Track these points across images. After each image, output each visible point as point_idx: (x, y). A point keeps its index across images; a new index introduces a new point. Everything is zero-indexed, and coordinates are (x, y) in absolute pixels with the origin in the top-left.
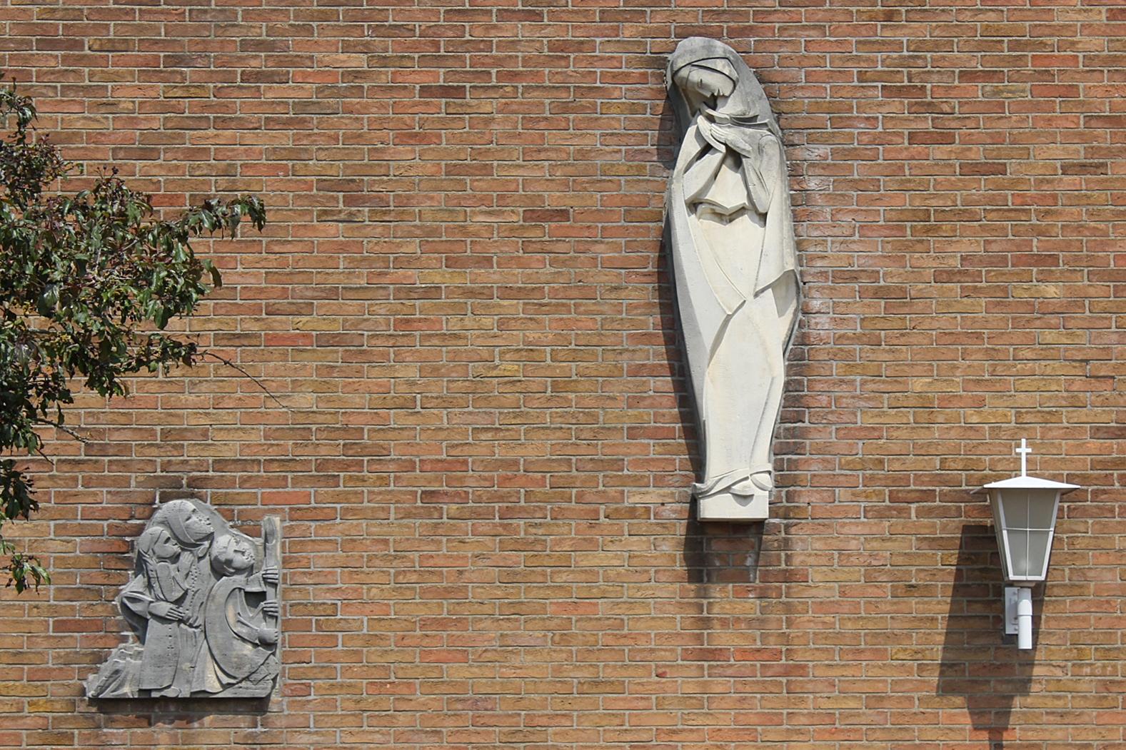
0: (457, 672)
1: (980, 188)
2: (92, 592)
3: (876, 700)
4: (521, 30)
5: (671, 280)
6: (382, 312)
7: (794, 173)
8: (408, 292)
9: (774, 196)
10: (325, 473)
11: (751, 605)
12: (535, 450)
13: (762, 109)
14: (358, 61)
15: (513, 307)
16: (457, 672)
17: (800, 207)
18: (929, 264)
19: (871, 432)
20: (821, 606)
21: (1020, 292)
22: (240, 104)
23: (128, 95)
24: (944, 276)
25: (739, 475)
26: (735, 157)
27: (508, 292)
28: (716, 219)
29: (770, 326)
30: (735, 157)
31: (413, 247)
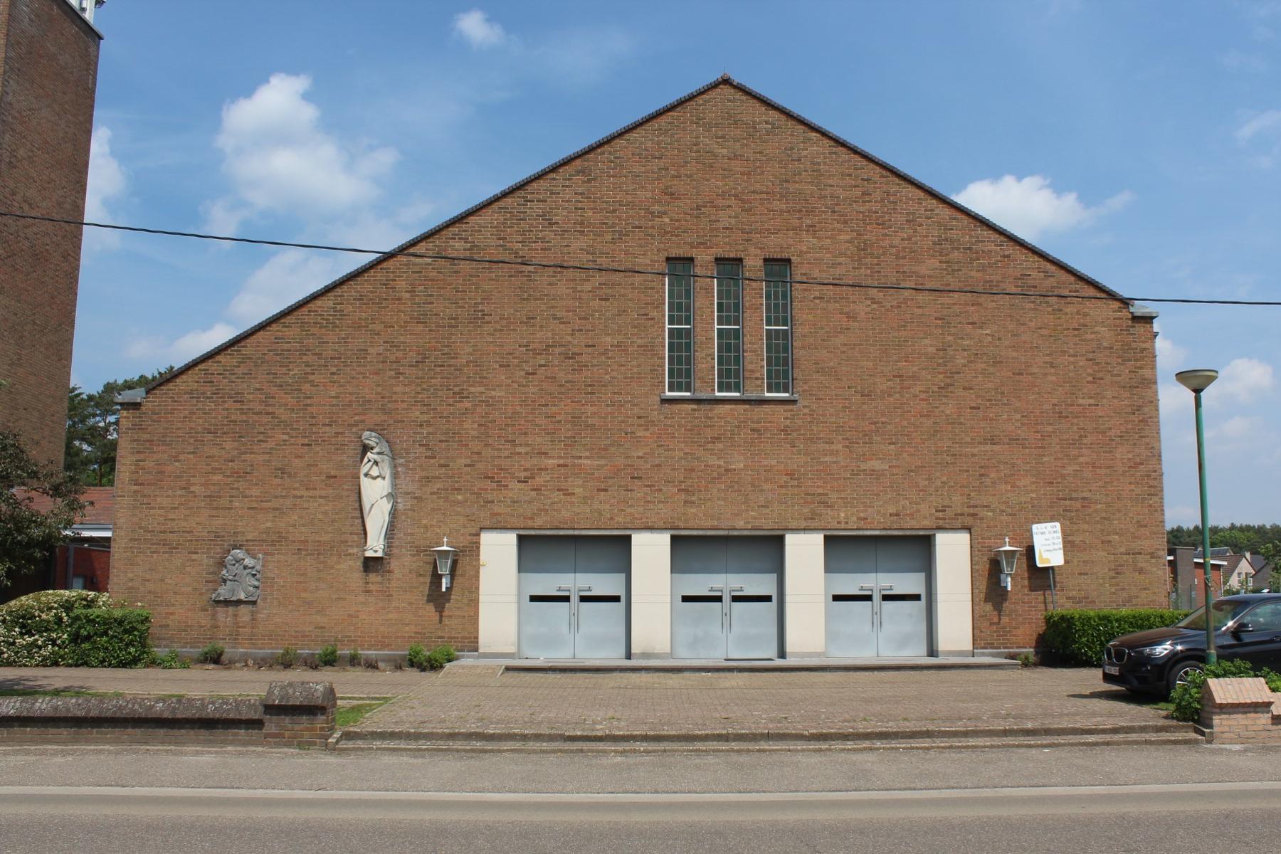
0: (304, 595)
1: (443, 470)
2: (214, 573)
3: (410, 604)
4: (327, 429)
5: (977, 632)
7: (395, 467)
8: (295, 497)
9: (387, 472)
10: (273, 544)
11: (379, 579)
12: (326, 538)
13: (386, 449)
14: (286, 437)
16: (304, 595)
17: (395, 475)
18: (429, 491)
19: (412, 534)
20: (398, 579)
21: (451, 498)
24: (432, 494)
25: (375, 545)
26: (376, 463)
27: (321, 497)
28: (983, 584)
29: (386, 506)
30: (376, 463)
31: (297, 485)
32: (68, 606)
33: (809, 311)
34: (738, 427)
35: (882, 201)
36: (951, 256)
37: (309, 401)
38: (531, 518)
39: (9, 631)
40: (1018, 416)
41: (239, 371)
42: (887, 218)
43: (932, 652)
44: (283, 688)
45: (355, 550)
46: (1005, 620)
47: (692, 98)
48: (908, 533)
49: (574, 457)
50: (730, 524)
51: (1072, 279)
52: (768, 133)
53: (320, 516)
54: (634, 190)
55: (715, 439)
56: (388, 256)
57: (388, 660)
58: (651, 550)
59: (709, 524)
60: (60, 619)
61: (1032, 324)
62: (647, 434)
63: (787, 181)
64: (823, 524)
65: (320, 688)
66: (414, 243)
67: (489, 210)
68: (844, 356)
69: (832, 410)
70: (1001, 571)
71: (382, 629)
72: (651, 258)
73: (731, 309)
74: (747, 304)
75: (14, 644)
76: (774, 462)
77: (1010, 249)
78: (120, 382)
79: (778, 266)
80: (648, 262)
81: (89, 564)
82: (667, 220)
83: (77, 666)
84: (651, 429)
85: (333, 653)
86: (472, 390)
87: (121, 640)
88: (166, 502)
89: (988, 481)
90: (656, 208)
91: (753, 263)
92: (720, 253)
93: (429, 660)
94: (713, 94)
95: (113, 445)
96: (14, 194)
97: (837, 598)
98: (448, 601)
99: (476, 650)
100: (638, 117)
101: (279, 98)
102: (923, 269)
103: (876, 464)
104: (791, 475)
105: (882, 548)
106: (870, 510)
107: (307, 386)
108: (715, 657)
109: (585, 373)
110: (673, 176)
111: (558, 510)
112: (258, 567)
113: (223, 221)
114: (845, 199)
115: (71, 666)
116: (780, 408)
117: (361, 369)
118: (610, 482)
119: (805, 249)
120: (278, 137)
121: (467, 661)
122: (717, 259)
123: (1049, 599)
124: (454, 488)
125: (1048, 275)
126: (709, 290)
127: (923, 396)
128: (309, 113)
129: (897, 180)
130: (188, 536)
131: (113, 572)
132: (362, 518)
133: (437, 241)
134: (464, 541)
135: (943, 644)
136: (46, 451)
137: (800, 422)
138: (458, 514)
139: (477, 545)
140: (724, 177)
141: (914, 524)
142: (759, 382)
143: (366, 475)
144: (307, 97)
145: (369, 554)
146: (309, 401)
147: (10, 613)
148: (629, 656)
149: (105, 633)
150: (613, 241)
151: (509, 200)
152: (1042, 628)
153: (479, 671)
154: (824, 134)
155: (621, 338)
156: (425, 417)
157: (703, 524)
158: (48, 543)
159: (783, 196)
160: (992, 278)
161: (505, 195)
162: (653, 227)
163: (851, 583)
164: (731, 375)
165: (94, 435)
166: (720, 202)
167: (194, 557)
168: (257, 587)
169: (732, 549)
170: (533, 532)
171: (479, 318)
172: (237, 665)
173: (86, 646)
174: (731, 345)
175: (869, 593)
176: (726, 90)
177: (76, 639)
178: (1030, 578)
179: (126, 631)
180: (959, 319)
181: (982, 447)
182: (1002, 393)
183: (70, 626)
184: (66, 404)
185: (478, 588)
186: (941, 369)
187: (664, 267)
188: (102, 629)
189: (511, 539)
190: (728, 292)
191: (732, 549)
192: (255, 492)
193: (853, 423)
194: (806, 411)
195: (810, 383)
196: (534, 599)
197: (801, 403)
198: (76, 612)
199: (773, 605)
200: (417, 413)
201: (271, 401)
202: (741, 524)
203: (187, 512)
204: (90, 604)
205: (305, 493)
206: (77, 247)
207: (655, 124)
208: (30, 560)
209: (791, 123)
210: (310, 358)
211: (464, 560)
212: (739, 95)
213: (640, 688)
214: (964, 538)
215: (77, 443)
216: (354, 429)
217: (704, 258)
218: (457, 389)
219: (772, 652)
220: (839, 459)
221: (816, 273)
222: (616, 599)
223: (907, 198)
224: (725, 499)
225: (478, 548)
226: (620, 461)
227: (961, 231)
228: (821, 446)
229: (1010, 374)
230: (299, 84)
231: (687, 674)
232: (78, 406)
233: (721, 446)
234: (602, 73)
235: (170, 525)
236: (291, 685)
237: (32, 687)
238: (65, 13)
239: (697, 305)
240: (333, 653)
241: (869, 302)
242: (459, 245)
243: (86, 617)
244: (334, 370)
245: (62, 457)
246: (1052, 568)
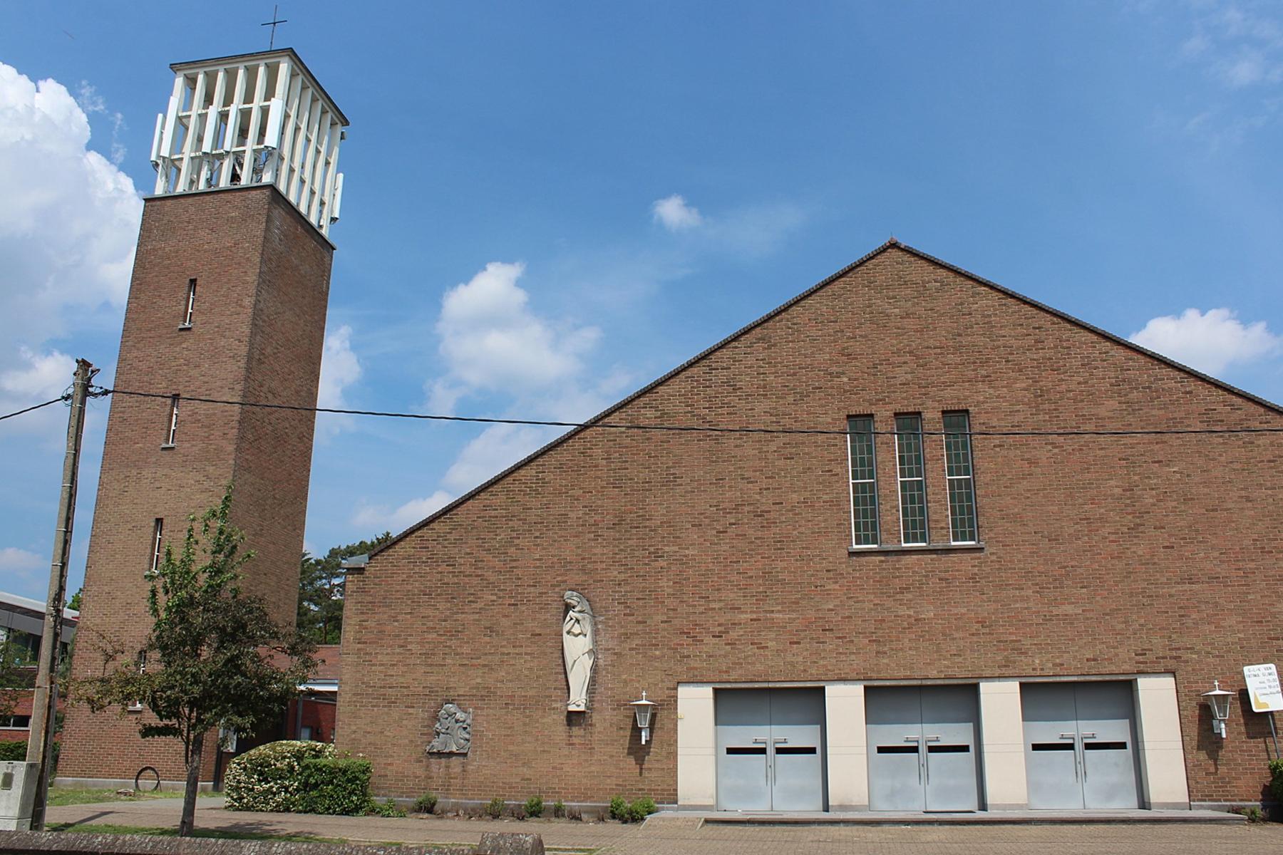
0: (511, 748)
1: (641, 627)
3: (612, 756)
4: (532, 589)
6: (497, 658)
8: (503, 654)
9: (588, 630)
10: (482, 698)
12: (531, 693)
13: (587, 608)
14: (494, 598)
15: (528, 658)
16: (511, 748)
17: (596, 633)
22: (467, 609)
23: (441, 606)
24: (631, 649)
25: (578, 700)
26: (578, 621)
28: (1194, 731)
29: (588, 662)
30: (578, 621)
32: (299, 756)
33: (987, 458)
34: (927, 576)
35: (1056, 347)
36: (1131, 396)
37: (514, 564)
39: (249, 778)
40: (1216, 554)
41: (451, 537)
42: (1061, 363)
43: (1144, 804)
44: (494, 839)
45: (559, 705)
46: (1223, 770)
47: (862, 263)
48: (1107, 678)
49: (766, 611)
50: (924, 673)
51: (1262, 410)
52: (938, 290)
53: (526, 673)
55: (903, 590)
56: (583, 428)
57: (590, 811)
58: (845, 702)
59: (901, 674)
60: (293, 768)
61: (1223, 459)
62: (837, 587)
63: (960, 335)
64: (1017, 671)
65: (529, 839)
66: (608, 414)
67: (677, 380)
68: (1028, 501)
69: (1020, 556)
70: (1213, 717)
71: (584, 781)
72: (832, 416)
73: (913, 461)
74: (928, 456)
75: (253, 789)
76: (964, 610)
77: (1192, 385)
78: (343, 547)
79: (956, 418)
81: (314, 716)
82: (845, 379)
83: (306, 812)
84: (841, 581)
85: (538, 804)
86: (666, 549)
87: (345, 789)
88: (385, 659)
89: (1189, 622)
90: (834, 369)
91: (932, 415)
92: (899, 408)
93: (630, 812)
94: (881, 258)
95: (339, 606)
96: (261, 386)
97: (1036, 747)
98: (648, 753)
99: (676, 803)
100: (812, 284)
101: (494, 285)
102: (1103, 412)
103: (1069, 609)
104: (982, 623)
105: (1085, 694)
106: (1066, 655)
107: (513, 549)
108: (914, 809)
109: (774, 530)
110: (849, 338)
111: (753, 664)
112: (469, 721)
113: (443, 401)
114: (1018, 349)
115: (300, 812)
116: (967, 556)
118: (802, 634)
119: (981, 398)
120: (491, 320)
121: (666, 813)
122: (896, 414)
123: (1271, 747)
124: (652, 643)
125: (1234, 408)
126: (890, 445)
127: (1112, 537)
128: (520, 296)
129: (1068, 326)
130: (405, 691)
131: (339, 724)
132: (566, 673)
133: (629, 410)
134: (663, 695)
135: (1155, 796)
136: (283, 615)
137: (988, 569)
138: (656, 669)
139: (675, 698)
140: (898, 335)
141: (1114, 669)
142: (944, 532)
143: (568, 632)
144: (519, 283)
145: (572, 708)
146: (514, 564)
147: (250, 761)
148: (826, 808)
149: (331, 782)
151: (695, 370)
152: (1268, 780)
153: (678, 823)
154: (992, 287)
156: (622, 576)
157: (897, 675)
158: (286, 696)
159: (957, 349)
160: (1175, 415)
161: (691, 365)
163: (1050, 732)
164: (916, 525)
165: (321, 596)
166: (896, 359)
167: (411, 710)
168: (468, 740)
169: (928, 699)
170: (728, 686)
171: (671, 481)
172: (450, 815)
173: (314, 793)
174: (915, 496)
175: (1071, 741)
176: (894, 253)
177: (306, 786)
178: (1246, 724)
179: (349, 781)
180: (1143, 459)
181: (1180, 587)
182: (1197, 531)
183: (300, 774)
184: (299, 570)
185: (676, 741)
186: (1130, 510)
187: (845, 425)
188: (328, 778)
189: (707, 692)
190: (909, 445)
191: (928, 699)
192: (466, 649)
193: (1041, 568)
194: (994, 558)
195: (996, 530)
196: (731, 751)
197: (988, 551)
198: (306, 761)
199: (972, 753)
200: (615, 573)
201: (480, 564)
202: (934, 673)
203: (405, 669)
204: (318, 754)
205: (511, 650)
206: (311, 429)
207: (829, 289)
208: (270, 713)
209: (959, 280)
210: (515, 523)
211: (662, 713)
212: (907, 257)
213: (839, 841)
214: (1169, 682)
215: (306, 604)
216: (557, 590)
217: (883, 414)
218: (652, 549)
219: (972, 804)
220: (1031, 605)
221: (994, 422)
222: (811, 751)
223: (1081, 343)
224: (916, 649)
225: (676, 701)
226: (811, 614)
227: (1139, 371)
228: (1011, 593)
229: (1203, 511)
230: (512, 271)
231: (886, 827)
232: (309, 570)
233: (910, 596)
234: (772, 242)
235: (392, 681)
236: (502, 835)
237: (269, 831)
238: (307, 231)
239: (879, 459)
240: (538, 804)
241: (1050, 447)
242: (650, 413)
243: (315, 766)
244: (538, 534)
245: (295, 618)
246: (1272, 713)
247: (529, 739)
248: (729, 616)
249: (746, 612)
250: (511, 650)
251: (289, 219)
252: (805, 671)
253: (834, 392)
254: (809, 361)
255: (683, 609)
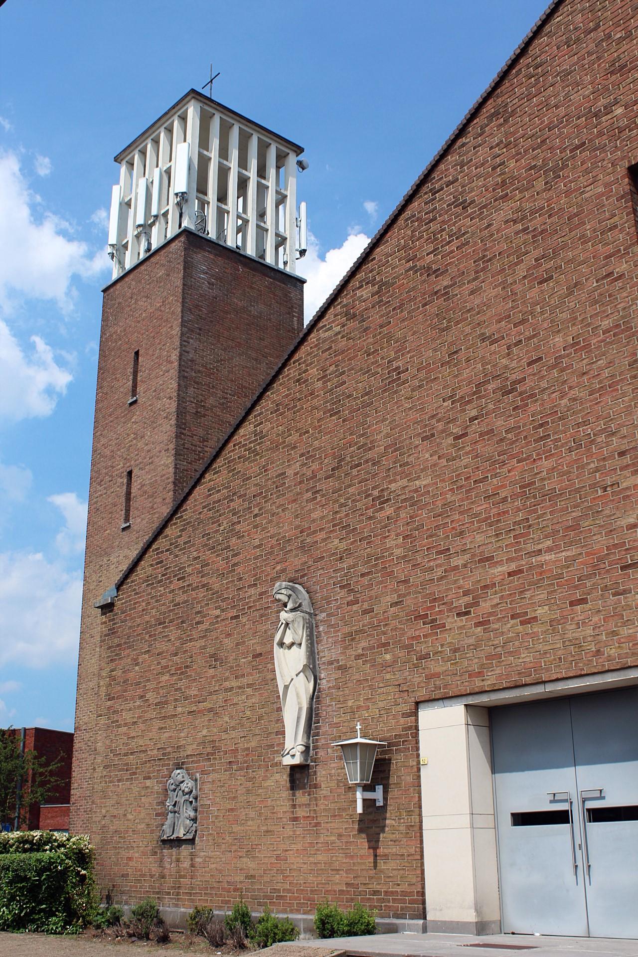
3: (340, 836)
4: (252, 591)
12: (253, 744)
14: (218, 612)
16: (236, 828)
24: (358, 657)
37: (236, 560)
38: (480, 674)
49: (530, 554)
54: (567, 96)
80: (601, 189)
86: (393, 486)
109: (533, 407)
111: (515, 653)
117: (279, 501)
134: (390, 727)
139: (415, 730)
143: (281, 644)
150: (548, 186)
155: (575, 330)
156: (343, 546)
161: (409, 200)
162: (601, 134)
196: (522, 819)
205: (234, 683)
210: (236, 504)
225: (416, 735)
226: (600, 542)
244: (256, 511)
247: (252, 814)
248: (478, 574)
249: (500, 563)
250: (234, 683)
251: (220, 261)
252: (598, 652)
253: (605, 140)
254: (562, 111)
255: (416, 578)
